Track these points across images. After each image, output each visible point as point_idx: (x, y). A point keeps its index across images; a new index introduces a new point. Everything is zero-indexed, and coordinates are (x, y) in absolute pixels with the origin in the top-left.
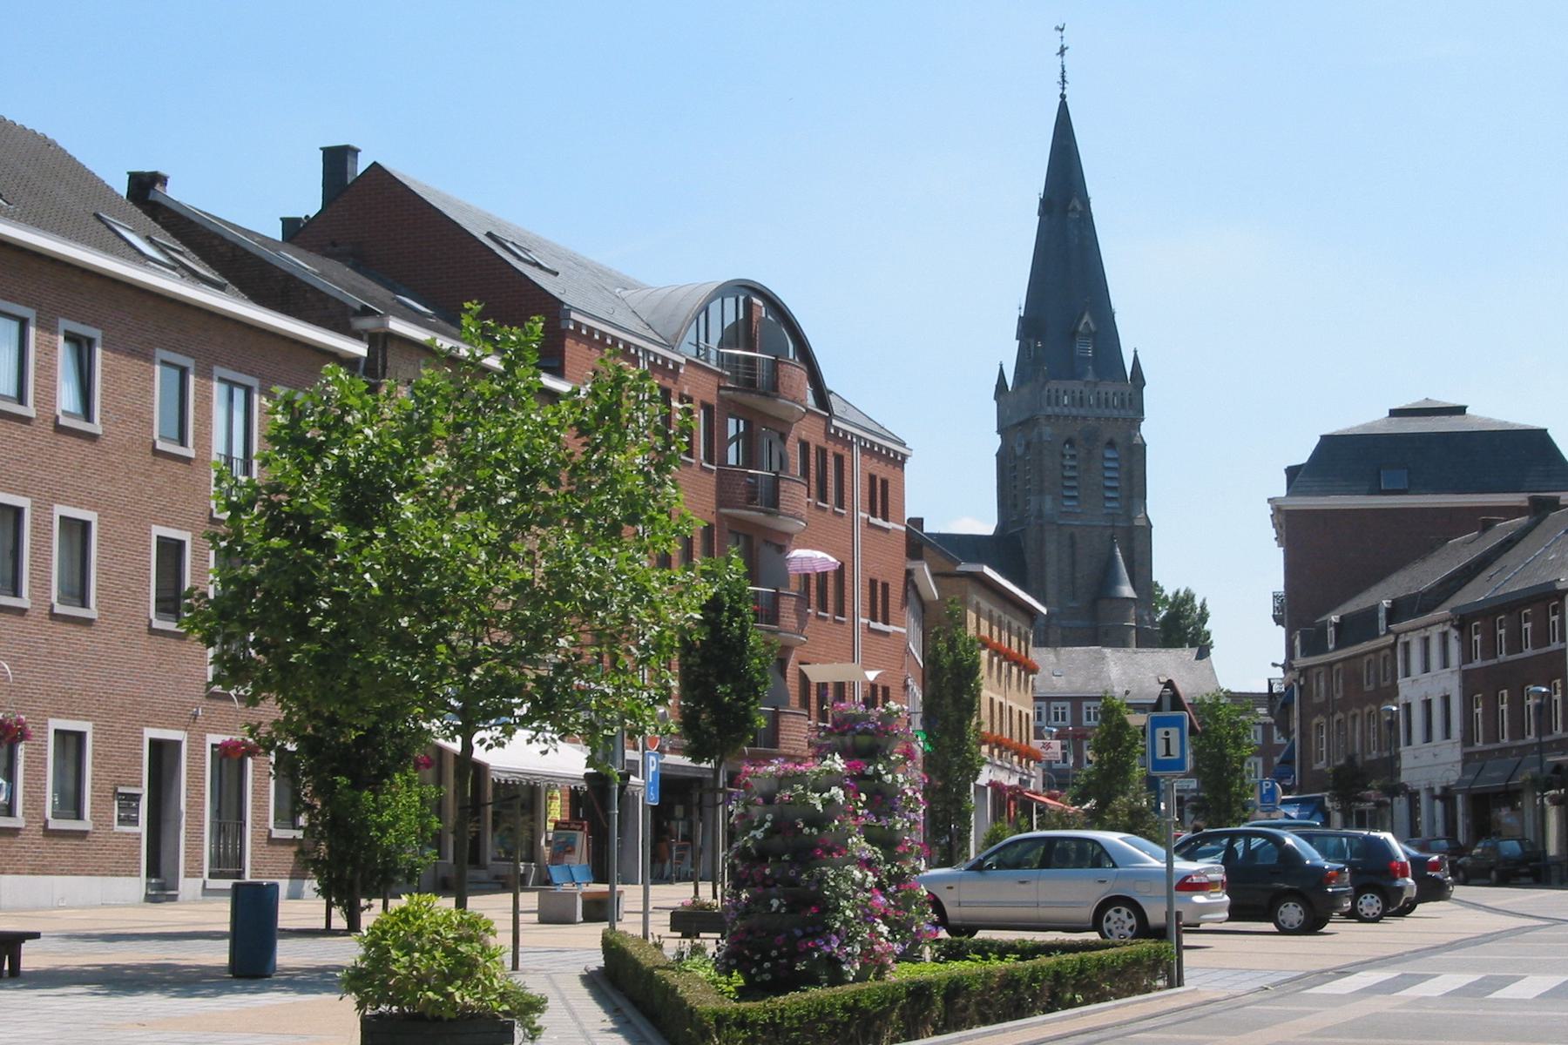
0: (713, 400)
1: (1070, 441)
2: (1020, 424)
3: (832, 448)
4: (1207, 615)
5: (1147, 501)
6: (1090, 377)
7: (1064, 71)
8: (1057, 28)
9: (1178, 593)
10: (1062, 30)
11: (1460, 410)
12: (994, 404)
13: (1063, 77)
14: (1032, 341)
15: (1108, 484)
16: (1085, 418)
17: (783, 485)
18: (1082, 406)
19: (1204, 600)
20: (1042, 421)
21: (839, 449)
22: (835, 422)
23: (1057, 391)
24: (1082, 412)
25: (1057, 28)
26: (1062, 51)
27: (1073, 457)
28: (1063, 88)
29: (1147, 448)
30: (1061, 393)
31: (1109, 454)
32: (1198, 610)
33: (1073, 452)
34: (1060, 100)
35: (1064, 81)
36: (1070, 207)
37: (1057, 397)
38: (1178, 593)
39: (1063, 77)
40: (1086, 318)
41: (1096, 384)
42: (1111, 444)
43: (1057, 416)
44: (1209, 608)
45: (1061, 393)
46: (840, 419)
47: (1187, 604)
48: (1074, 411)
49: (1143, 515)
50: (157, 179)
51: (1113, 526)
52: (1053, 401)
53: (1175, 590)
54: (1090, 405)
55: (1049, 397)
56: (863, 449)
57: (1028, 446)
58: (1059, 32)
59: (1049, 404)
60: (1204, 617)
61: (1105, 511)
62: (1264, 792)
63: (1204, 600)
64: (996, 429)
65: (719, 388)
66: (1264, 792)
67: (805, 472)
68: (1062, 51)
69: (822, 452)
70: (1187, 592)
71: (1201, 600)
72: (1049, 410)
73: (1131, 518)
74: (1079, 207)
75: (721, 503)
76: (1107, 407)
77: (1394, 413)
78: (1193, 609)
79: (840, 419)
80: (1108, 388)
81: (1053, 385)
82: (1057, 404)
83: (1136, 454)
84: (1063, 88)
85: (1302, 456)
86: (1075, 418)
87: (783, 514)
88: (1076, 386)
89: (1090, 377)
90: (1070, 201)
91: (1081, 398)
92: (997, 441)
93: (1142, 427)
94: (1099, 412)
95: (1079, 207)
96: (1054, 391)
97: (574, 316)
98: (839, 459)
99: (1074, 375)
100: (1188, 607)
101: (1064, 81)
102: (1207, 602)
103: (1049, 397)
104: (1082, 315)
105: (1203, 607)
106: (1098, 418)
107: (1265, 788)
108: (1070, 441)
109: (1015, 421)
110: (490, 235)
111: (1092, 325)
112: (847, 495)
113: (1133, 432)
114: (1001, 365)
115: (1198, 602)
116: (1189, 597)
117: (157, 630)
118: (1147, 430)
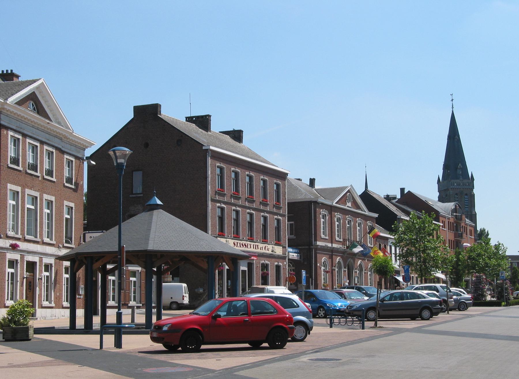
0: (453, 222)
1: (457, 194)
2: (445, 190)
3: (465, 226)
4: (489, 234)
5: (475, 208)
6: (461, 179)
7: (453, 105)
8: (451, 95)
9: (481, 229)
10: (452, 95)
12: (437, 185)
13: (453, 106)
14: (447, 170)
15: (466, 204)
16: (460, 188)
17: (463, 234)
18: (459, 186)
19: (488, 230)
20: (450, 189)
21: (466, 226)
22: (466, 222)
23: (453, 182)
24: (459, 187)
25: (451, 95)
26: (452, 100)
27: (457, 198)
28: (453, 109)
29: (475, 195)
30: (454, 182)
31: (466, 197)
32: (486, 233)
33: (457, 197)
34: (452, 112)
35: (453, 107)
36: (455, 138)
37: (453, 184)
38: (481, 229)
39: (453, 106)
40: (460, 165)
41: (463, 180)
42: (466, 195)
43: (454, 188)
44: (489, 232)
45: (454, 182)
46: (467, 221)
47: (484, 231)
48: (457, 187)
49: (474, 211)
50: (155, 109)
51: (467, 214)
52: (452, 185)
53: (480, 228)
54: (461, 185)
55: (451, 184)
56: (469, 225)
57: (446, 195)
58: (451, 96)
59: (451, 185)
60: (488, 235)
61: (465, 210)
62: (406, 269)
63: (488, 230)
64: (438, 191)
65: (454, 220)
66: (406, 269)
67: (465, 232)
68: (452, 100)
69: (464, 227)
70: (483, 229)
71: (487, 231)
72: (452, 187)
73: (471, 212)
74: (457, 138)
75: (455, 237)
76: (465, 186)
78: (485, 233)
79: (467, 221)
80: (465, 181)
81: (453, 181)
82: (453, 185)
83: (472, 197)
84: (453, 109)
86: (458, 189)
87: (464, 239)
88: (458, 181)
89: (461, 179)
90: (455, 137)
91: (459, 184)
92: (438, 194)
93: (474, 190)
94: (463, 187)
95: (457, 138)
96: (452, 182)
97: (441, 213)
98: (466, 227)
99: (457, 178)
100: (484, 232)
101: (453, 107)
102: (489, 231)
103: (451, 184)
104: (459, 164)
105: (488, 232)
106: (463, 188)
107: (406, 268)
108: (457, 194)
109: (443, 189)
110: (425, 201)
111: (461, 166)
112: (445, 226)
113: (471, 191)
114: (439, 176)
115: (486, 231)
116: (484, 230)
117: (45, 243)
118: (475, 191)
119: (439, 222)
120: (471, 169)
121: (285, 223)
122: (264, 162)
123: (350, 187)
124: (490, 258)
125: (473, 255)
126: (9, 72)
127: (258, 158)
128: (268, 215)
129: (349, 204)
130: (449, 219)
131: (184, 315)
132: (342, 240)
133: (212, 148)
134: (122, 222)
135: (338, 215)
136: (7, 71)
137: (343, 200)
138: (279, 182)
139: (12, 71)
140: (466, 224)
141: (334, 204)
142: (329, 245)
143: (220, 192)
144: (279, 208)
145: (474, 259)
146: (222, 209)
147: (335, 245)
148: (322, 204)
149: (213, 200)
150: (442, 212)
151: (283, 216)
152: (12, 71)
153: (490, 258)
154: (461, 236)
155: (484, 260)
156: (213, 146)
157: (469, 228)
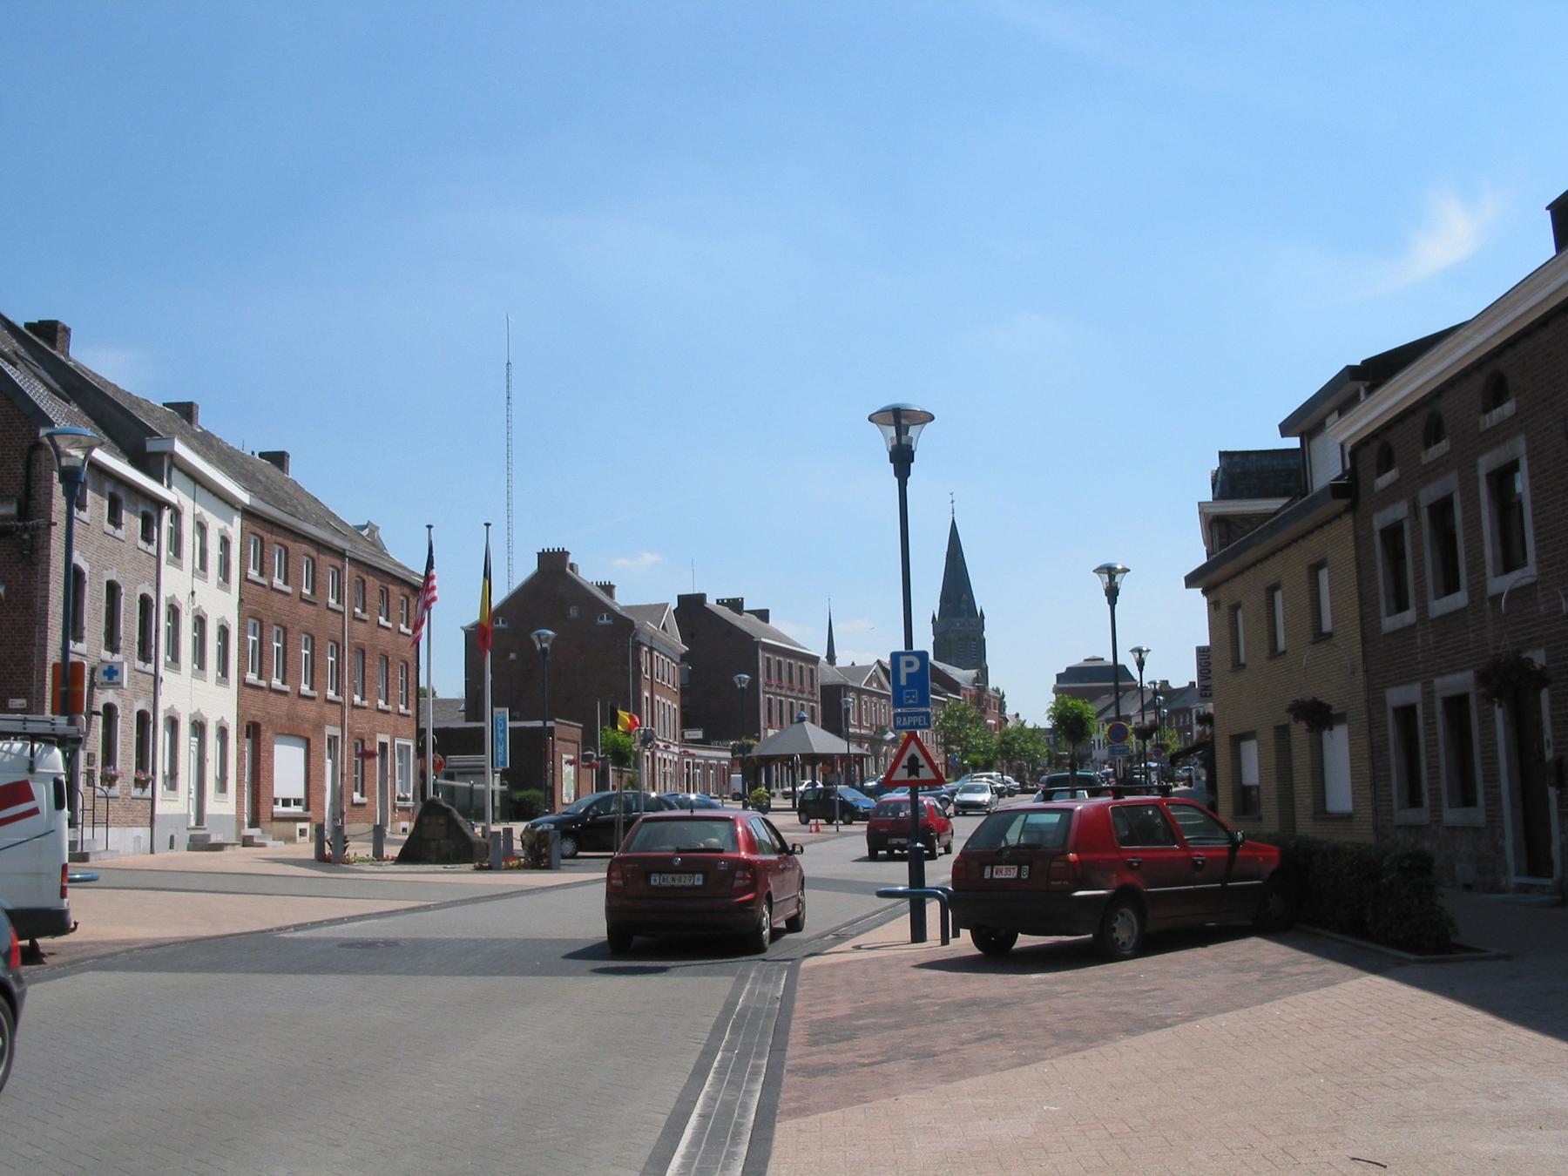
11: (1102, 659)
26: (952, 502)
35: (953, 513)
48: (961, 628)
68: (952, 502)
77: (1085, 660)
80: (973, 620)
85: (1063, 670)
119: (959, 695)
120: (980, 603)
121: (818, 708)
122: (794, 646)
123: (875, 666)
124: (1025, 742)
125: (1008, 739)
126: (607, 584)
127: (788, 641)
128: (804, 703)
129: (875, 685)
130: (970, 691)
131: (422, 622)
132: (869, 725)
133: (763, 640)
134: (54, 346)
135: (865, 697)
136: (559, 549)
137: (869, 683)
138: (813, 667)
139: (563, 549)
140: (989, 696)
141: (862, 686)
142: (858, 731)
143: (768, 684)
144: (813, 694)
145: (1008, 743)
146: (770, 700)
147: (863, 731)
148: (852, 687)
149: (765, 692)
150: (964, 684)
151: (817, 702)
152: (563, 549)
153: (1025, 742)
154: (984, 711)
155: (1019, 744)
156: (765, 638)
157: (992, 700)
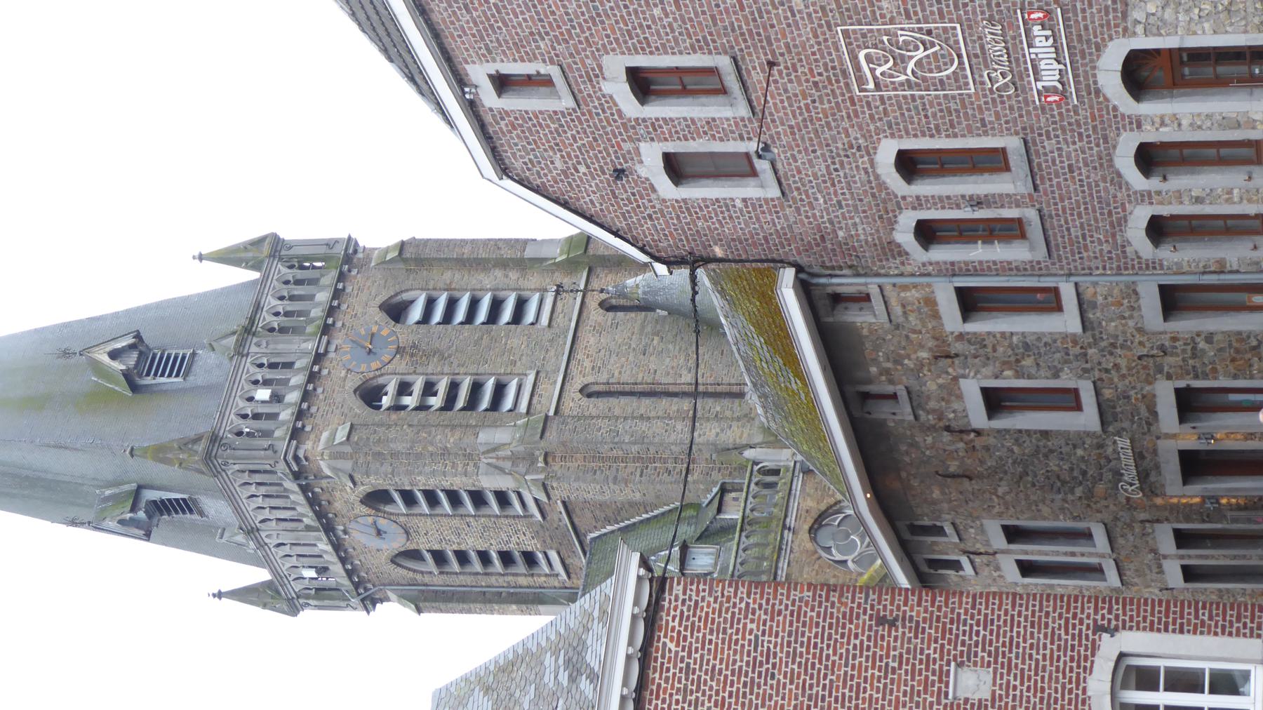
48: (297, 379)
